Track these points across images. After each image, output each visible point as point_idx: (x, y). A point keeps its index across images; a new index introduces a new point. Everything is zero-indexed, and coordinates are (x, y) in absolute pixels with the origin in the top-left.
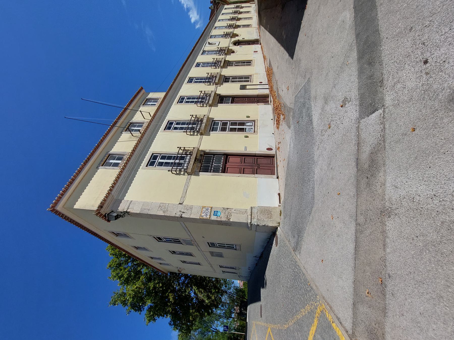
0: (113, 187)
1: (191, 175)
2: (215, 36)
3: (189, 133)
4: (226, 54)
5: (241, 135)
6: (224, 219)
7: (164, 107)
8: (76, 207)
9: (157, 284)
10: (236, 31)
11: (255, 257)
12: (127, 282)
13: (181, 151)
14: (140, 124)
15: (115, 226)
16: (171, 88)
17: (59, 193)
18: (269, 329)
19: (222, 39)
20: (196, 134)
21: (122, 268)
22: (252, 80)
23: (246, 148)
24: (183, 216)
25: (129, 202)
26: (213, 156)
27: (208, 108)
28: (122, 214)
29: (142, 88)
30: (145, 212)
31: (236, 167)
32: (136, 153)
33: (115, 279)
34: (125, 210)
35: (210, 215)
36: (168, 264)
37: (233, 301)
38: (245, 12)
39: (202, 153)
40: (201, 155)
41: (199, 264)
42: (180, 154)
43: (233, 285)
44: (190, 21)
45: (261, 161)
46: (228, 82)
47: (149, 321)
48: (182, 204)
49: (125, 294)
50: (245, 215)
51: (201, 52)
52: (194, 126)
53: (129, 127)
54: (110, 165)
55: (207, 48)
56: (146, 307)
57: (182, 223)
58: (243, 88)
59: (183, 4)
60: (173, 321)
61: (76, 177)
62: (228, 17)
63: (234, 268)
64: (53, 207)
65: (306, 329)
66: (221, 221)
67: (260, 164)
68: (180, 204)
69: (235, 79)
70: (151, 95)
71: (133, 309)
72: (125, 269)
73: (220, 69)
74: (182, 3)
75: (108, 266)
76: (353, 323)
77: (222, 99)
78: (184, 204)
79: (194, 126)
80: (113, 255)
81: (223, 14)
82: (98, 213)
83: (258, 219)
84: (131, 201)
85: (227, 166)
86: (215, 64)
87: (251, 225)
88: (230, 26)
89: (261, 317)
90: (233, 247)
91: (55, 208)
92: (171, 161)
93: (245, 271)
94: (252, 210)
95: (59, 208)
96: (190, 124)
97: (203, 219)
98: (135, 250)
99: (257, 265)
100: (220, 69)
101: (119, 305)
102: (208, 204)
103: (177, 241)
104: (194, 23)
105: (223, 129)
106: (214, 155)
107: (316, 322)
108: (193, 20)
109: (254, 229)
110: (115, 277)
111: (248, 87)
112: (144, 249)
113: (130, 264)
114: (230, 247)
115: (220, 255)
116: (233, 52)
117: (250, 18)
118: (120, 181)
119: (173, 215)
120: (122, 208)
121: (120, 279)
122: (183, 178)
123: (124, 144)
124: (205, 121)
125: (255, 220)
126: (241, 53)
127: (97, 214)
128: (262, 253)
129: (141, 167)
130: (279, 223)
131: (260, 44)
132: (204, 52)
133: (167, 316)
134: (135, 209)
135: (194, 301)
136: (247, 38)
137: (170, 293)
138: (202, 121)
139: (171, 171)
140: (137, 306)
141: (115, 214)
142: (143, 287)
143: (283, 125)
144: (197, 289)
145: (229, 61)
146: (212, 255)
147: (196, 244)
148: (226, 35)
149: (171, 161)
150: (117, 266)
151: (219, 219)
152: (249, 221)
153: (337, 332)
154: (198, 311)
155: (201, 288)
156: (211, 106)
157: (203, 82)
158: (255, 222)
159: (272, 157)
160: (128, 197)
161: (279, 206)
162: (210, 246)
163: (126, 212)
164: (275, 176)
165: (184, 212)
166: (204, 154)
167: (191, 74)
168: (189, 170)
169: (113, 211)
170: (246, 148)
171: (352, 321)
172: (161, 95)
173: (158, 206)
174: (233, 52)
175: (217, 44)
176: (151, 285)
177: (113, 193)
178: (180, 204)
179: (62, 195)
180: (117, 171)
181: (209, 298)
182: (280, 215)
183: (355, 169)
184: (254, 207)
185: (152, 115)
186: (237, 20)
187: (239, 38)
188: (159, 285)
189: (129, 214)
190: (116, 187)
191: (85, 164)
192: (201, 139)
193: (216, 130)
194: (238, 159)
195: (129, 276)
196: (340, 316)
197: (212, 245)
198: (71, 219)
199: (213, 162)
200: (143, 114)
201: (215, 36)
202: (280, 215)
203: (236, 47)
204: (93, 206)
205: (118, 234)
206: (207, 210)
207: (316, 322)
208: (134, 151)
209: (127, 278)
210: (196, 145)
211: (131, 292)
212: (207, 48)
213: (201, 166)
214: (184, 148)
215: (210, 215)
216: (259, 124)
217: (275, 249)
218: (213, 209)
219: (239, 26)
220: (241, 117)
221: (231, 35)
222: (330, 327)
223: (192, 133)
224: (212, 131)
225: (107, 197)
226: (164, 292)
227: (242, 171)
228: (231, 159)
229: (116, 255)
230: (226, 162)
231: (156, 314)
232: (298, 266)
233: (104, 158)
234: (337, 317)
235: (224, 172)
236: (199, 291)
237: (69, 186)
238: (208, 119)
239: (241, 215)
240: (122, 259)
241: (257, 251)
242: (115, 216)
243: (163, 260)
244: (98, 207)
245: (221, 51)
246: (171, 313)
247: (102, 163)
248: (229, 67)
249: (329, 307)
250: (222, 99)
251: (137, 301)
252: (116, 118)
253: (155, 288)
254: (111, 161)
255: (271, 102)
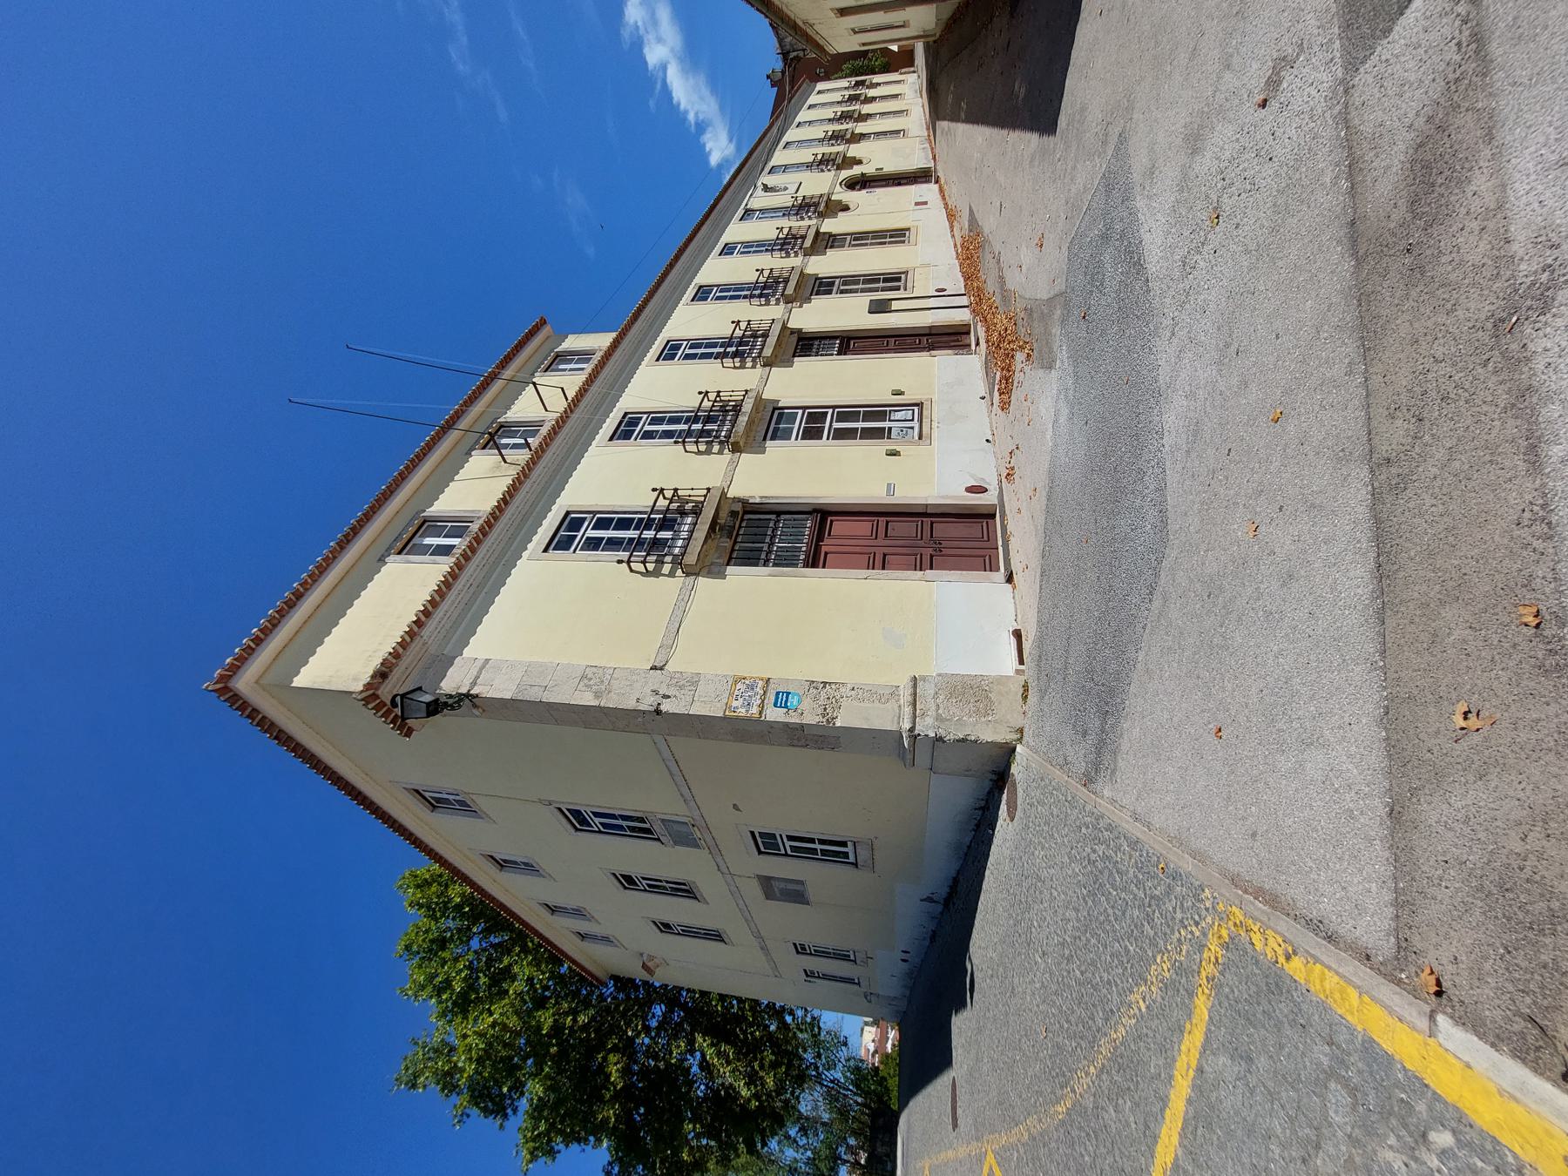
0: (426, 613)
1: (697, 574)
2: (785, 168)
3: (693, 448)
4: (822, 215)
5: (877, 448)
6: (811, 718)
7: (608, 374)
8: (298, 682)
9: (566, 1014)
10: (854, 150)
11: (929, 900)
12: (463, 1005)
13: (662, 503)
14: (530, 428)
15: (429, 757)
16: (635, 322)
17: (248, 634)
18: (991, 1159)
19: (808, 174)
20: (716, 448)
21: (446, 955)
22: (909, 285)
23: (890, 489)
24: (663, 708)
25: (479, 664)
26: (773, 517)
27: (759, 370)
28: (450, 701)
29: (543, 322)
30: (533, 695)
31: (858, 549)
32: (510, 510)
33: (424, 994)
34: (464, 690)
35: (762, 706)
36: (606, 940)
37: (843, 1113)
38: (883, 98)
39: (738, 507)
40: (734, 514)
41: (716, 936)
42: (658, 512)
43: (843, 1053)
44: (707, 162)
45: (943, 529)
46: (830, 292)
47: (534, 1157)
48: (661, 669)
49: (453, 1049)
50: (892, 705)
51: (740, 212)
52: (710, 425)
53: (492, 438)
54: (424, 550)
55: (759, 200)
56: (524, 1104)
57: (659, 739)
58: (879, 307)
59: (686, 112)
60: (620, 1160)
61: (307, 586)
62: (829, 113)
63: (845, 958)
64: (222, 678)
65: (1155, 1063)
66: (802, 726)
67: (948, 536)
68: (654, 668)
69: (850, 284)
70: (572, 343)
71: (477, 1104)
72: (456, 960)
73: (800, 258)
74: (682, 107)
75: (400, 948)
76: (1396, 904)
77: (807, 344)
78: (669, 667)
79: (710, 425)
80: (421, 906)
81: (810, 107)
82: (370, 696)
83: (938, 718)
84: (487, 661)
85: (824, 549)
86: (786, 244)
87: (914, 737)
88: (836, 137)
89: (955, 1126)
90: (846, 855)
91: (231, 684)
92: (631, 534)
93: (887, 971)
94: (915, 686)
95: (244, 683)
96: (696, 420)
97: (737, 718)
98: (492, 869)
99: (933, 936)
100: (800, 258)
101: (430, 1090)
102: (756, 669)
103: (639, 828)
104: (720, 166)
105: (812, 433)
106: (779, 514)
107: (1202, 1006)
108: (714, 159)
109: (922, 757)
110: (423, 987)
111: (895, 305)
112: (529, 868)
113: (475, 944)
114: (834, 851)
115: (795, 894)
116: (846, 208)
117: (898, 132)
118: (452, 596)
119: (630, 704)
120: (454, 681)
121: (439, 995)
122: (670, 586)
123: (475, 486)
124: (747, 407)
125: (929, 720)
126: (869, 210)
127: (366, 701)
128: (955, 881)
129: (525, 554)
130: (1021, 731)
131: (937, 182)
132: (748, 213)
133: (599, 1141)
134: (497, 687)
135: (701, 1090)
136: (890, 167)
137: (610, 1051)
138: (737, 409)
139: (629, 562)
140: (490, 1098)
141: (428, 698)
142: (513, 1022)
143: (1028, 377)
144: (712, 1045)
145: (830, 235)
146: (769, 895)
147: (711, 843)
148: (823, 163)
149: (631, 534)
150: (430, 950)
151: (794, 719)
152: (907, 725)
153: (1315, 987)
154: (711, 1133)
155: (727, 1043)
156: (768, 364)
157: (745, 297)
158: (927, 727)
159: (985, 516)
160: (476, 648)
161: (1017, 672)
162: (760, 852)
163: (468, 695)
164: (1001, 575)
165: (666, 697)
166: (746, 512)
167: (702, 278)
168: (691, 559)
169: (420, 689)
170: (890, 489)
171: (1388, 896)
172: (600, 341)
173: (579, 674)
174: (846, 208)
175: (792, 189)
176: (546, 1019)
177: (426, 632)
178: (654, 668)
179: (258, 641)
180: (444, 565)
181: (752, 1079)
182: (1025, 698)
183: (1348, 264)
184: (924, 679)
185: (571, 394)
186: (857, 120)
187: (868, 169)
188: (575, 1020)
189: (475, 706)
190: (439, 614)
191: (342, 548)
192: (734, 466)
193: (786, 435)
194: (863, 527)
195: (471, 985)
196: (1325, 907)
197: (767, 843)
198: (281, 731)
199: (773, 537)
200: (540, 400)
201: (785, 168)
202: (1025, 698)
203: (855, 193)
204: (355, 679)
205: (438, 800)
206: (751, 687)
207: (1202, 1006)
208: (505, 501)
209: (464, 995)
210: (716, 482)
211: (473, 1040)
212: (759, 200)
213: (733, 550)
214: (676, 490)
215: (762, 706)
216: (936, 412)
217: (1005, 830)
218: (772, 686)
219: (862, 137)
220: (877, 394)
221: (839, 160)
222: (1276, 984)
223: (702, 447)
224: (772, 438)
225: (403, 644)
226: (591, 1049)
227: (879, 561)
228: (839, 527)
229: (429, 908)
230: (819, 535)
231: (561, 1132)
232: (1110, 828)
233: (405, 529)
234: (1308, 922)
235: (814, 565)
236: (719, 1054)
237: (282, 614)
238: (760, 402)
239: (877, 704)
240: (451, 924)
241: (936, 873)
242: (428, 704)
243: (590, 919)
244: (373, 677)
245: (804, 207)
246: (613, 1133)
247: (399, 545)
248: (830, 252)
249: (1266, 903)
250: (807, 344)
251: (492, 1076)
252: (458, 414)
253: (557, 1029)
254: (428, 541)
255: (978, 344)
